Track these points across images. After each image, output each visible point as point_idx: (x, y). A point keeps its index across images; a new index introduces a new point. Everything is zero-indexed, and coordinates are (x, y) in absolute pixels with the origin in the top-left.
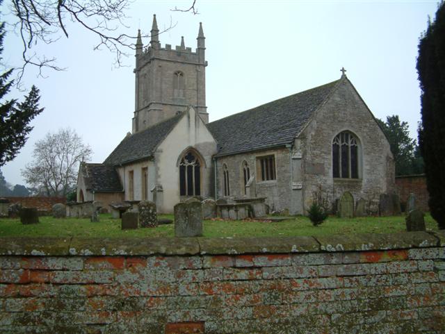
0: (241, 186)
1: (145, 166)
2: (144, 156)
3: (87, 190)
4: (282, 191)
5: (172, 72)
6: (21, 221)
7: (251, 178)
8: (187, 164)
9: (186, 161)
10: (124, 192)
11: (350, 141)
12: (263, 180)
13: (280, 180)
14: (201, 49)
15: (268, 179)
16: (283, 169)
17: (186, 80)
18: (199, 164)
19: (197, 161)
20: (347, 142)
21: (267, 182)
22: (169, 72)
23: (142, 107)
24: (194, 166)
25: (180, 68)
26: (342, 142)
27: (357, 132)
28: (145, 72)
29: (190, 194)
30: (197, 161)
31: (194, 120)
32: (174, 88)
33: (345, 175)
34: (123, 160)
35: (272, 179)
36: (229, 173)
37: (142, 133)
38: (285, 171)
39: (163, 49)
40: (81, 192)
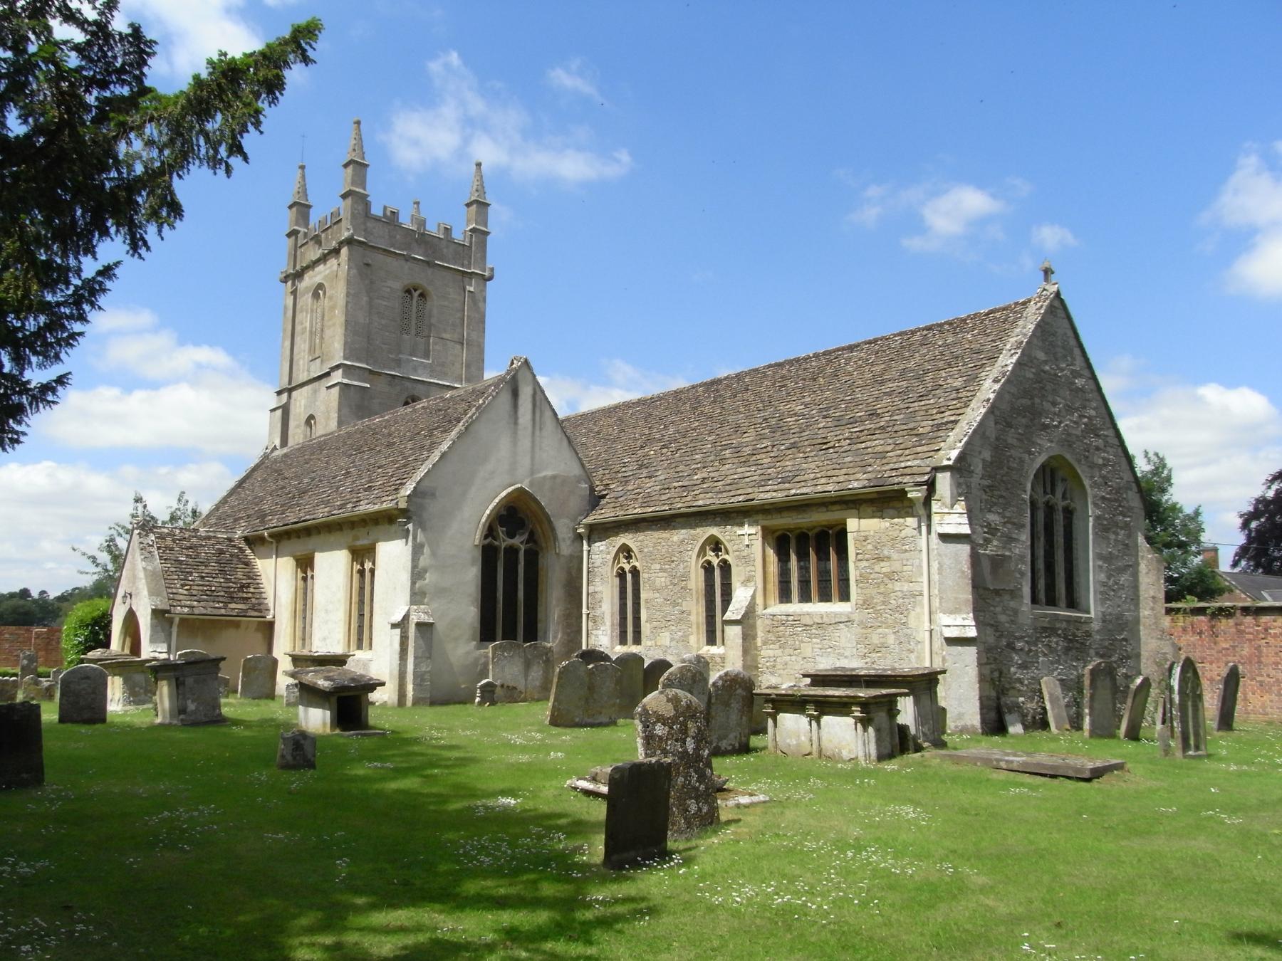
0: (693, 618)
1: (363, 542)
2: (366, 508)
3: (157, 614)
4: (875, 639)
5: (398, 285)
6: (39, 716)
7: (741, 596)
8: (504, 542)
9: (501, 531)
10: (271, 625)
11: (1059, 494)
12: (785, 596)
13: (866, 604)
14: (480, 235)
15: (805, 597)
16: (885, 567)
17: (435, 311)
18: (535, 542)
19: (532, 534)
20: (1053, 492)
21: (807, 607)
22: (390, 283)
23: (302, 376)
24: (523, 548)
25: (421, 277)
26: (1045, 493)
27: (1079, 461)
28: (318, 279)
29: (1051, 601)
30: (532, 534)
31: (530, 406)
32: (405, 329)
33: (510, 634)
34: (274, 522)
35: (825, 597)
36: (644, 576)
37: (301, 450)
38: (892, 576)
39: (377, 219)
40: (131, 618)
